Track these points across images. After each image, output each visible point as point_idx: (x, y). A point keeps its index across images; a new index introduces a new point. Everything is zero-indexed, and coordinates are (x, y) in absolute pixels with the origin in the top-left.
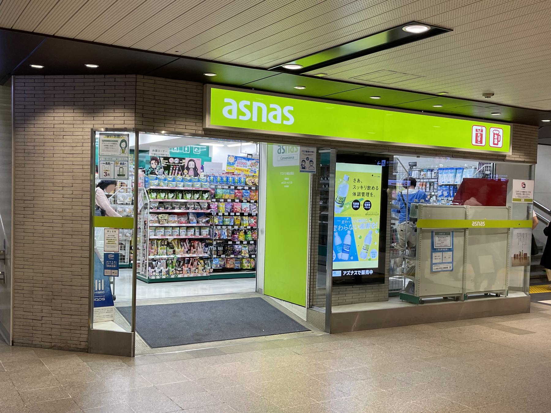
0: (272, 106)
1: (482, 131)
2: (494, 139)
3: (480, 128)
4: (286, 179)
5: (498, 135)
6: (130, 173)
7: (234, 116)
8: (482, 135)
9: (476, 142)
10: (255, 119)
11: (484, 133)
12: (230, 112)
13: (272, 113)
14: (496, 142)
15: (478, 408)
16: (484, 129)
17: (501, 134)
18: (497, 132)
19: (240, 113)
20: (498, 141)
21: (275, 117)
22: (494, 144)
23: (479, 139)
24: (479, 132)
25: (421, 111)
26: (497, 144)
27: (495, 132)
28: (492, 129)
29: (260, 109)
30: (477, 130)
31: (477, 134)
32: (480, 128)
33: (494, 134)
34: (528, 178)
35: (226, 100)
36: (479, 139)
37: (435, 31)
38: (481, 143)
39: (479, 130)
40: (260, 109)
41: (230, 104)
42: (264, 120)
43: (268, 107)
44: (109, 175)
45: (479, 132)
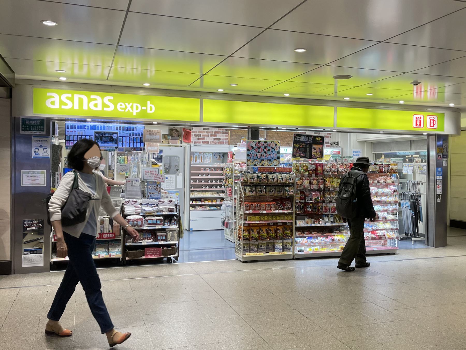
0: (92, 97)
1: (421, 118)
2: (430, 123)
3: (419, 116)
5: (433, 120)
7: (99, 108)
8: (420, 121)
9: (417, 125)
10: (76, 107)
14: (432, 125)
15: (235, 229)
16: (422, 117)
17: (436, 119)
18: (433, 119)
20: (434, 124)
21: (96, 105)
22: (430, 126)
23: (418, 123)
24: (418, 119)
26: (433, 126)
27: (431, 118)
28: (429, 117)
29: (81, 101)
30: (416, 118)
31: (417, 121)
32: (419, 116)
33: (430, 120)
34: (50, 330)
35: (49, 94)
36: (418, 123)
38: (420, 125)
40: (81, 101)
41: (96, 100)
42: (85, 107)
45: (418, 119)
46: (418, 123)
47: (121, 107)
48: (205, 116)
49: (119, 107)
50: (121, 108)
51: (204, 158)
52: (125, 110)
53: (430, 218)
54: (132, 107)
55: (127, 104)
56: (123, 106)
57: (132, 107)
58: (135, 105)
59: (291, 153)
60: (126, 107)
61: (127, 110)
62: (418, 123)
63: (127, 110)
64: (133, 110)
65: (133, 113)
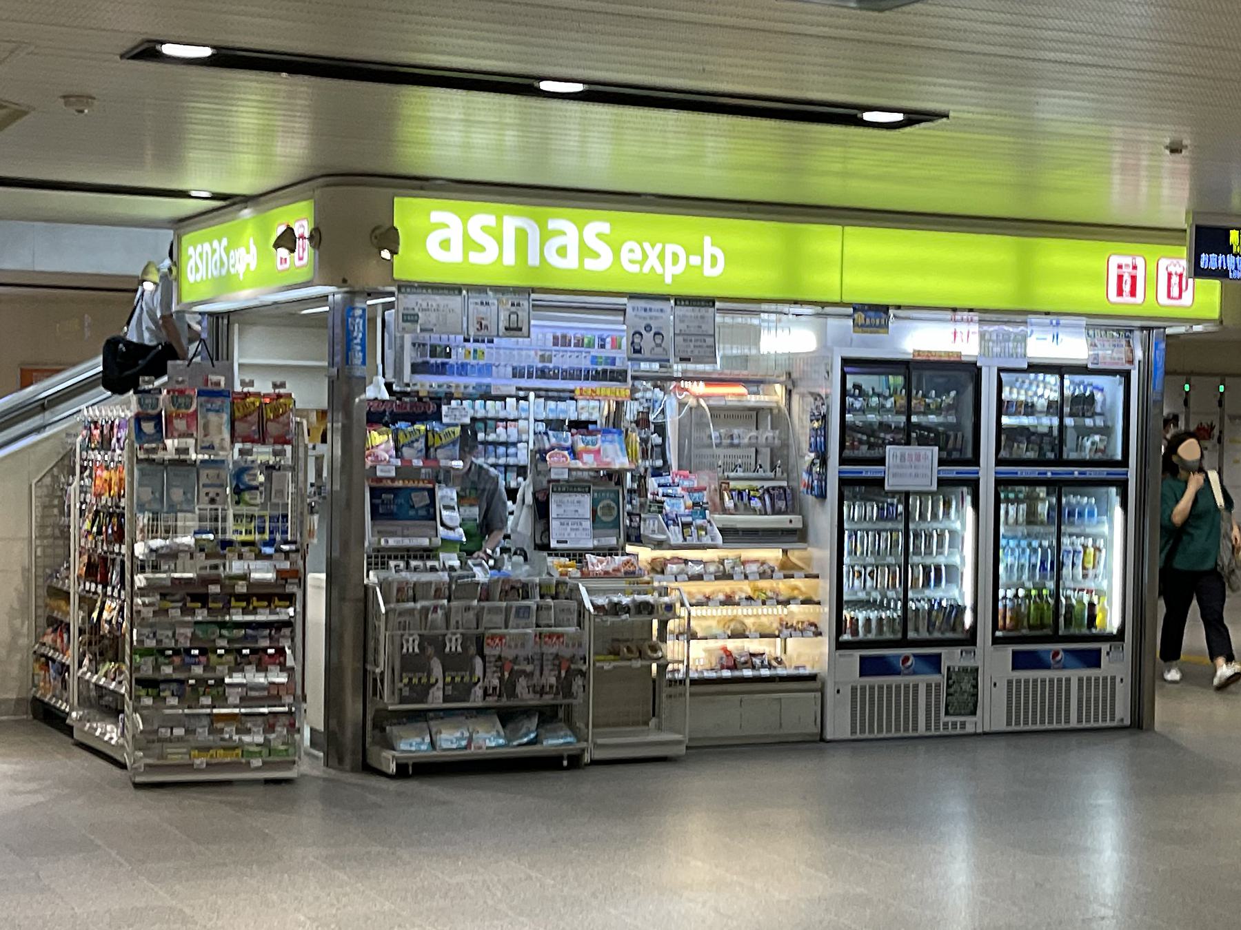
1: (1135, 268)
3: (1129, 261)
4: (219, 651)
6: (452, 337)
8: (1134, 278)
9: (1120, 292)
10: (509, 258)
11: (1140, 274)
12: (445, 244)
13: (556, 242)
14: (1175, 292)
16: (1140, 262)
19: (470, 244)
23: (1127, 288)
25: (443, 288)
30: (1120, 267)
31: (1120, 277)
36: (1127, 288)
37: (914, 118)
38: (1133, 293)
39: (1127, 266)
40: (521, 235)
43: (542, 227)
44: (486, 327)
46: (1127, 285)
47: (632, 256)
48: (847, 279)
49: (625, 256)
50: (631, 261)
51: (817, 315)
52: (642, 266)
53: (825, 240)
54: (661, 257)
55: (647, 246)
56: (638, 255)
57: (661, 257)
58: (670, 248)
59: (840, 228)
60: (645, 256)
61: (646, 269)
62: (1127, 285)
63: (646, 269)
64: (663, 265)
65: (663, 276)
